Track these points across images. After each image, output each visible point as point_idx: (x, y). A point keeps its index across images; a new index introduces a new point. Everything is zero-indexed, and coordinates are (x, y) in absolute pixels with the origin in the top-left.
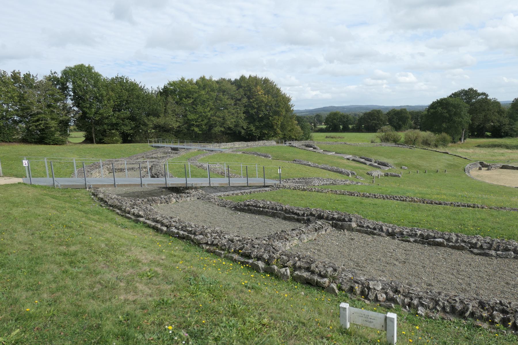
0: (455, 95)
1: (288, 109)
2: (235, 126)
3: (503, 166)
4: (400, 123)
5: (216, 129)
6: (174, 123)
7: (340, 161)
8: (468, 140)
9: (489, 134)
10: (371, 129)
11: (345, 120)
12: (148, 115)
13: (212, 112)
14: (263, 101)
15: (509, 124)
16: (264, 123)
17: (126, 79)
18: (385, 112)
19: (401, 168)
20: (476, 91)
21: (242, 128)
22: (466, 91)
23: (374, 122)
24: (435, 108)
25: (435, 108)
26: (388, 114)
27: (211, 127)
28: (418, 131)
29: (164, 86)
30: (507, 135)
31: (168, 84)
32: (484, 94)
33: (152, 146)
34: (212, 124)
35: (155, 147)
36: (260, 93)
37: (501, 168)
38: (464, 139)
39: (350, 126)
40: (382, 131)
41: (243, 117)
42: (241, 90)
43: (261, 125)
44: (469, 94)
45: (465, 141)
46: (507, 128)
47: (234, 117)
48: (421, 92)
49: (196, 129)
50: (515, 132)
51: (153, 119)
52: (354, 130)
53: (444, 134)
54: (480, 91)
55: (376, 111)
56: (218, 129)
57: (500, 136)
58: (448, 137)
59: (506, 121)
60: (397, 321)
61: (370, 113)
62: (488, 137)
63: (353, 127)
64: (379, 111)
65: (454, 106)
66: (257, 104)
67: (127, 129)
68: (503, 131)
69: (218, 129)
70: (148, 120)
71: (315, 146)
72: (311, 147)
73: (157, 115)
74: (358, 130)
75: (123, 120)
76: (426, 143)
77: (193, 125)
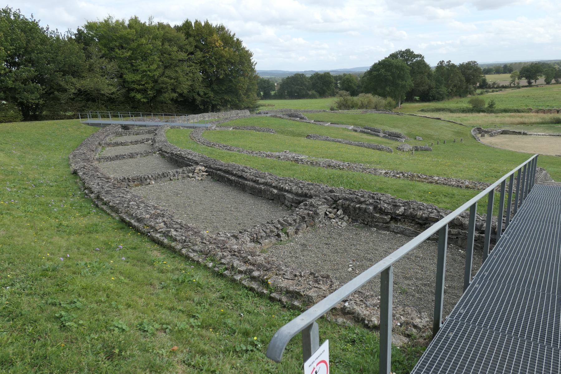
0: (393, 56)
1: (253, 70)
2: (189, 92)
3: (503, 131)
4: (324, 88)
5: (166, 95)
6: (107, 87)
7: (346, 133)
8: (404, 105)
9: (417, 98)
10: (322, 94)
11: (266, 86)
12: (65, 73)
13: (161, 70)
14: (222, 56)
15: (436, 88)
16: (225, 87)
17: (14, 14)
18: (308, 76)
19: (415, 139)
20: (413, 52)
21: (199, 95)
22: (404, 52)
23: (298, 87)
24: (378, 70)
25: (378, 70)
26: (312, 78)
27: (159, 92)
28: (370, 95)
29: (79, 30)
30: (434, 99)
31: (86, 27)
32: (420, 56)
33: (88, 124)
34: (162, 88)
35: (92, 125)
36: (217, 44)
37: (502, 134)
38: (401, 104)
39: (273, 93)
40: (341, 96)
41: (201, 79)
42: (191, 39)
43: (221, 90)
44: (408, 54)
45: (402, 105)
46: (434, 91)
47: (188, 78)
48: (358, 55)
49: (139, 96)
50: (441, 95)
51: (74, 80)
52: (276, 97)
53: (389, 99)
54: (416, 52)
55: (299, 74)
56: (168, 96)
57: (429, 100)
58: (394, 103)
59: (433, 84)
60: (332, 290)
61: (292, 77)
62: (417, 101)
63: (275, 93)
64: (303, 75)
65: (397, 67)
66: (216, 59)
67: (33, 98)
68: (430, 94)
69: (168, 96)
70: (67, 82)
71: (303, 116)
72: (296, 116)
73: (76, 74)
74: (280, 96)
75: (25, 82)
76: (376, 108)
77: (133, 90)
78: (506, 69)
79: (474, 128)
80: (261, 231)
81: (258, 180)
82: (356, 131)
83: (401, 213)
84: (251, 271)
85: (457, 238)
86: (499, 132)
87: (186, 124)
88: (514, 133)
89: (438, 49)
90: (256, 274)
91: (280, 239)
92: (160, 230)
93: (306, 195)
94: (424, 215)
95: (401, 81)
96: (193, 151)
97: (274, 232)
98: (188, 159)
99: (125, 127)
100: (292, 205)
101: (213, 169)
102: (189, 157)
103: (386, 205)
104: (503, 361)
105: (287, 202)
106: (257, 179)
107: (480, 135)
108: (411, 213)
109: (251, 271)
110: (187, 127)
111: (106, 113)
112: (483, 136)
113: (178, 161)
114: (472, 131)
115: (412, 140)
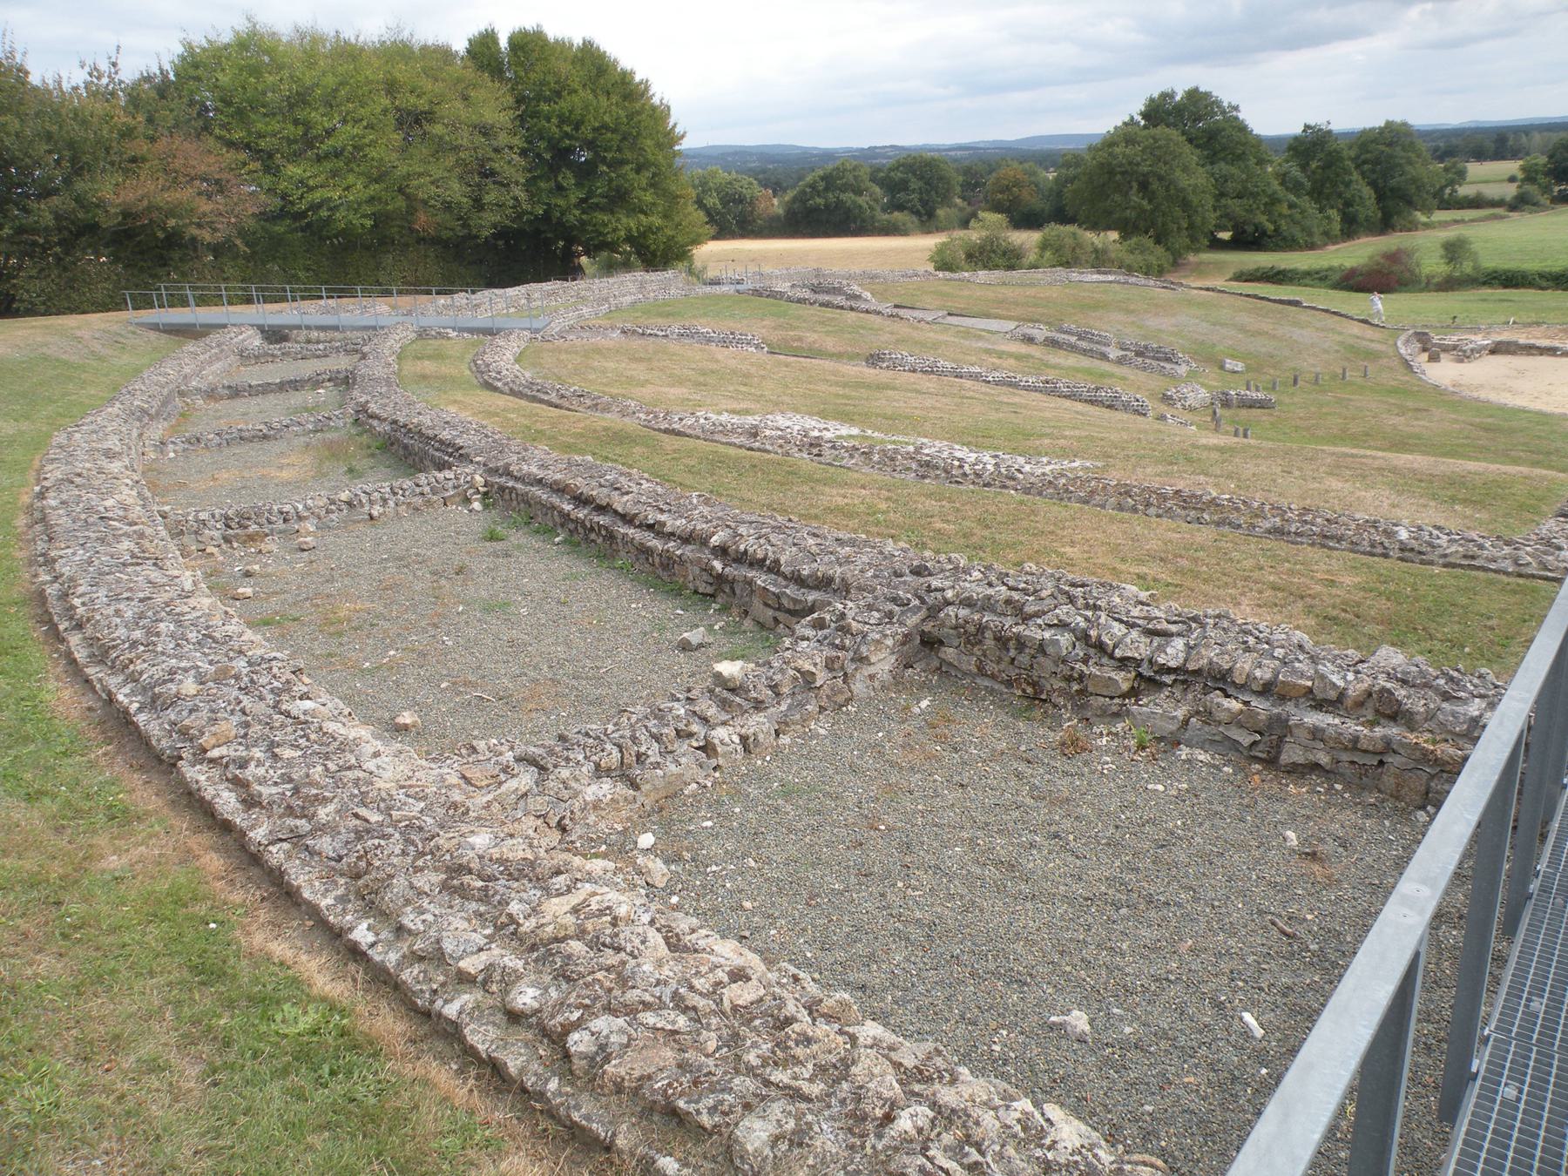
3: (1499, 343)
37: (1493, 352)
78: (1496, 143)
79: (1403, 338)
80: (643, 736)
81: (663, 524)
82: (1030, 340)
83: (1173, 664)
84: (510, 980)
85: (1381, 763)
86: (1484, 347)
87: (467, 319)
88: (1530, 350)
89: (1277, 101)
90: (526, 997)
91: (713, 762)
92: (215, 753)
93: (824, 583)
94: (1258, 673)
95: (1173, 190)
96: (454, 413)
97: (691, 735)
98: (442, 442)
99: (275, 335)
100: (776, 620)
101: (517, 479)
102: (446, 435)
103: (1118, 629)
104: (1475, 1135)
105: (757, 604)
106: (662, 518)
107: (1425, 356)
108: (1211, 662)
109: (510, 980)
110: (471, 331)
111: (244, 289)
112: (1434, 358)
113: (409, 451)
114: (1399, 344)
115: (1211, 372)
